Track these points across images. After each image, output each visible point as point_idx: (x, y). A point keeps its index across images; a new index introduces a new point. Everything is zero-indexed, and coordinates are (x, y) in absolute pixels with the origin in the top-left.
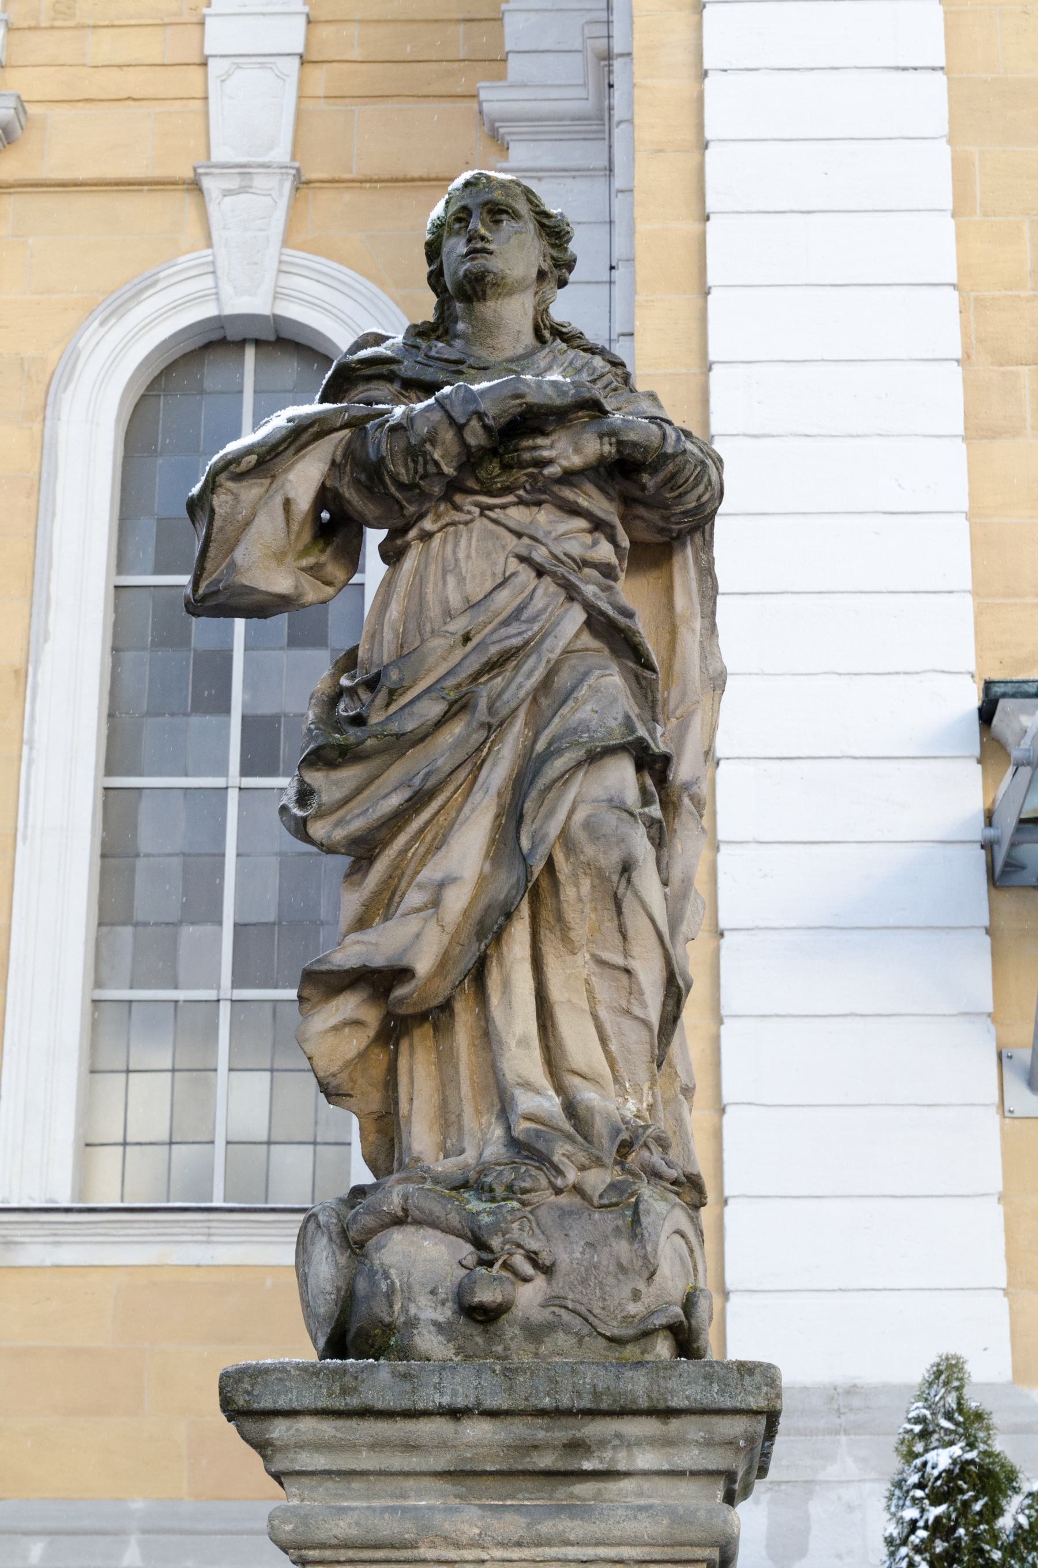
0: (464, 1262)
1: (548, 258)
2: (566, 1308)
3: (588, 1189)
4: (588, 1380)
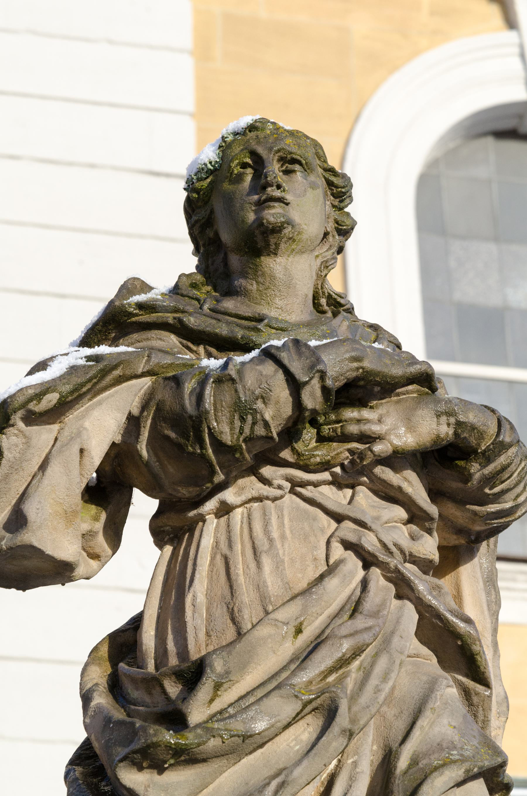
1: (331, 220)
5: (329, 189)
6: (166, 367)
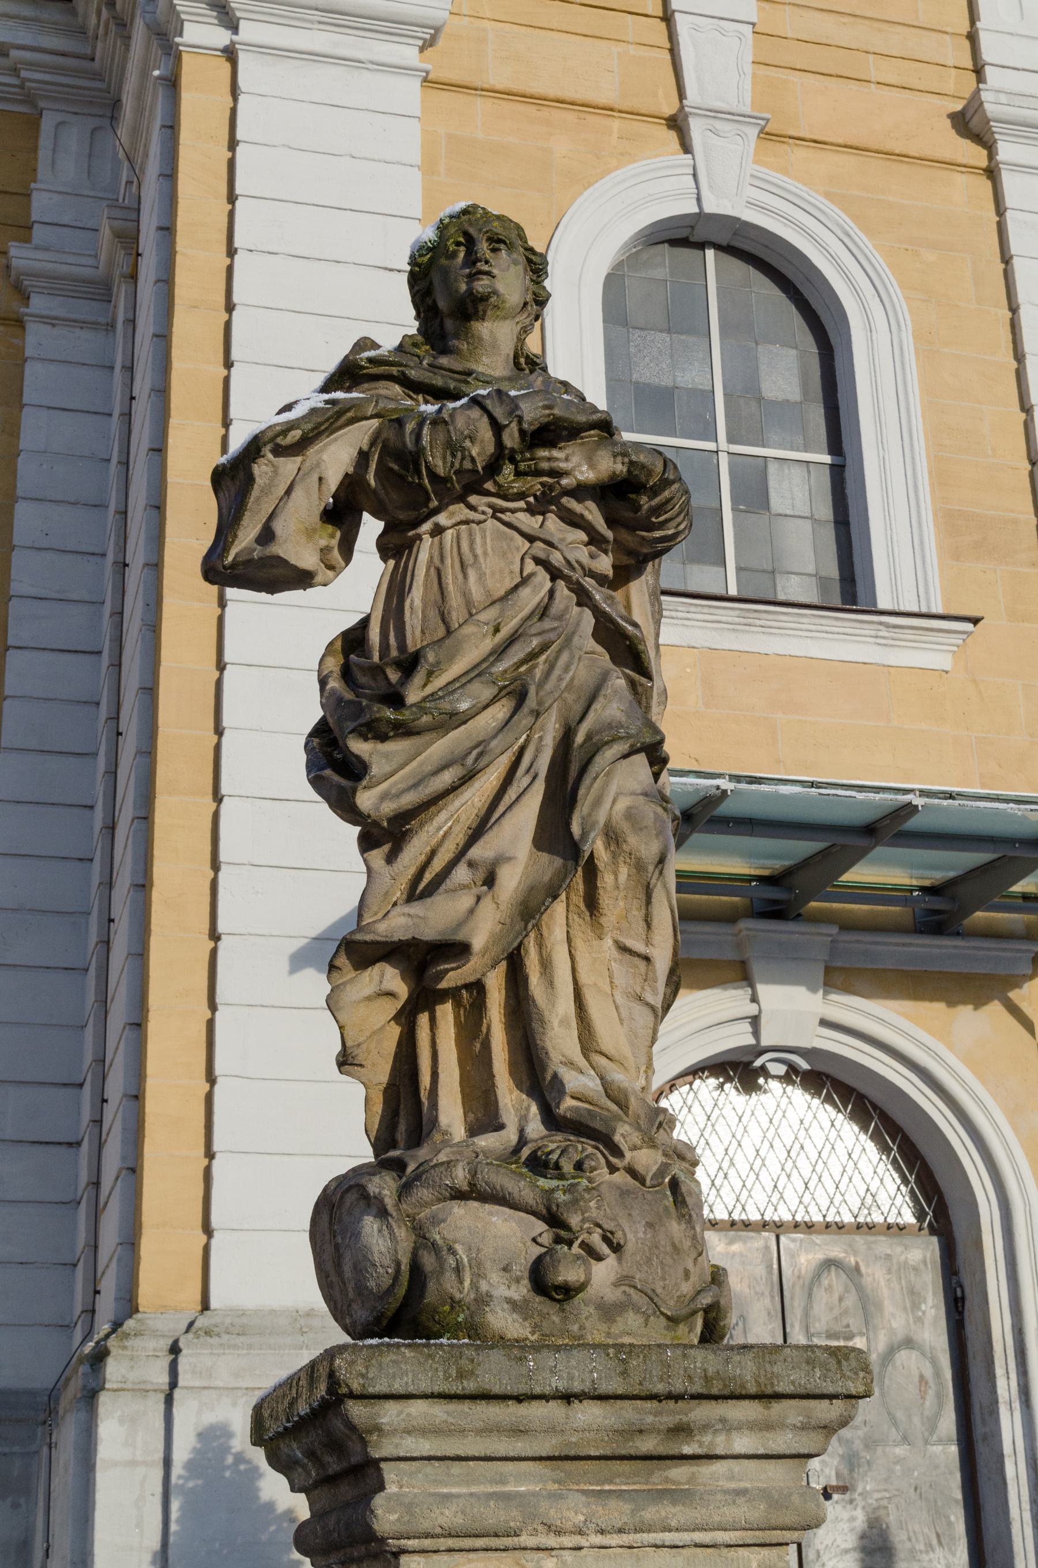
0: (539, 1240)
2: (635, 1288)
3: (640, 1168)
4: (698, 1365)
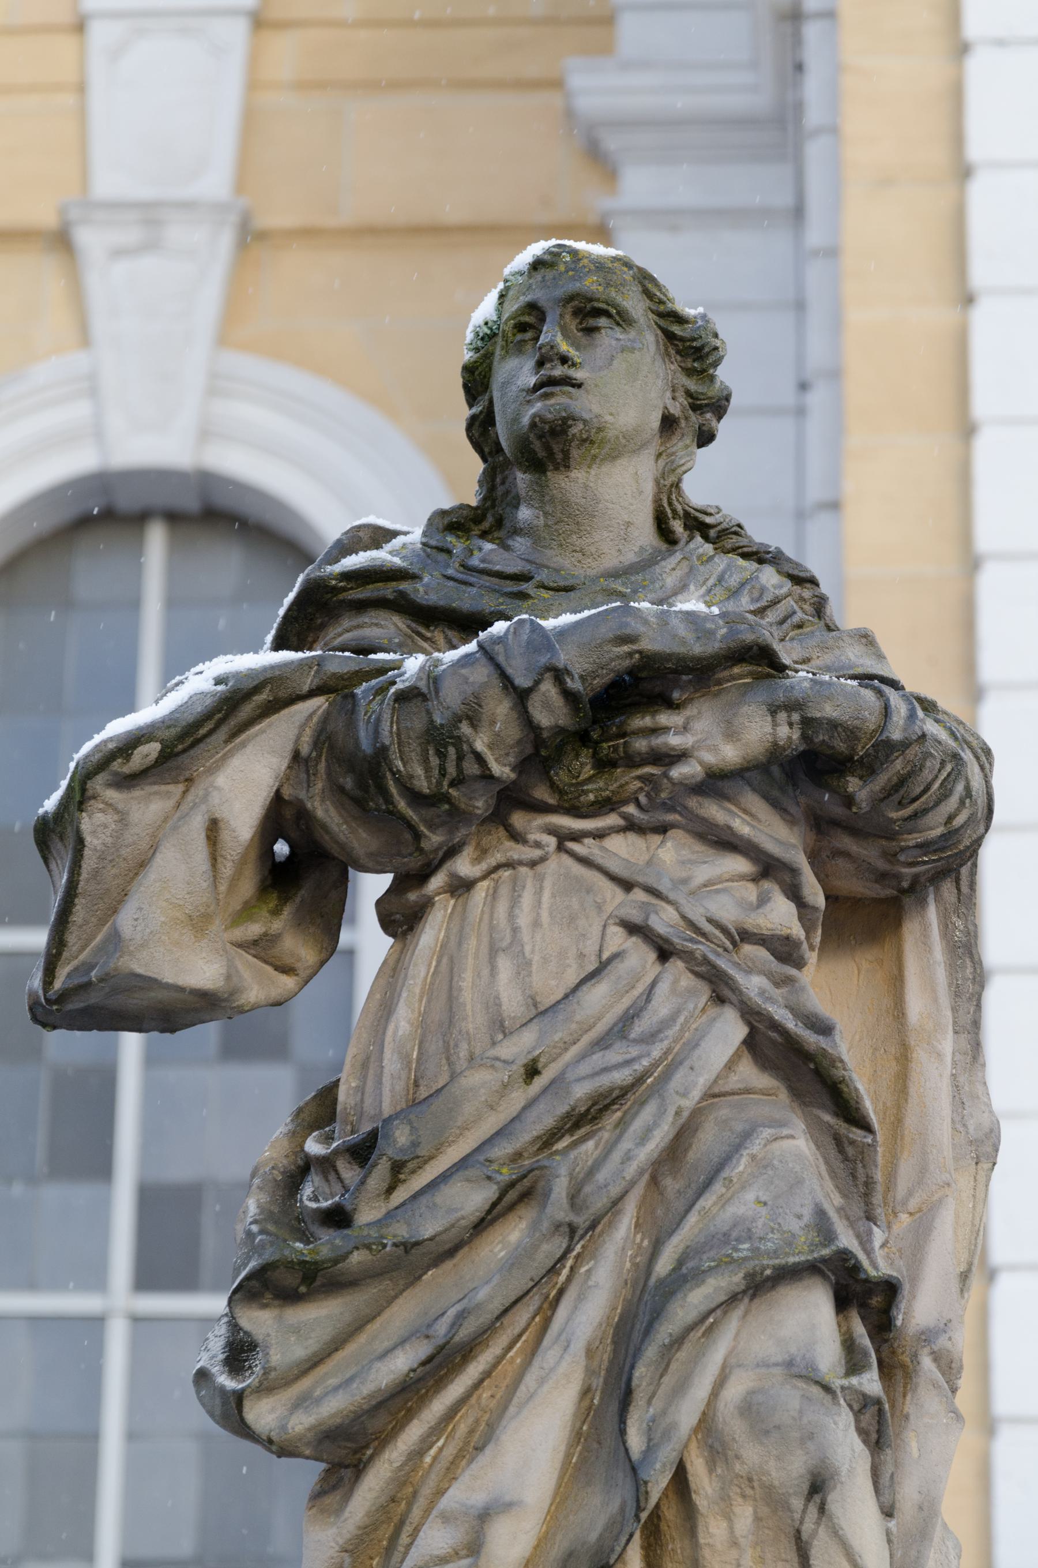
5: (672, 344)
6: (349, 678)
